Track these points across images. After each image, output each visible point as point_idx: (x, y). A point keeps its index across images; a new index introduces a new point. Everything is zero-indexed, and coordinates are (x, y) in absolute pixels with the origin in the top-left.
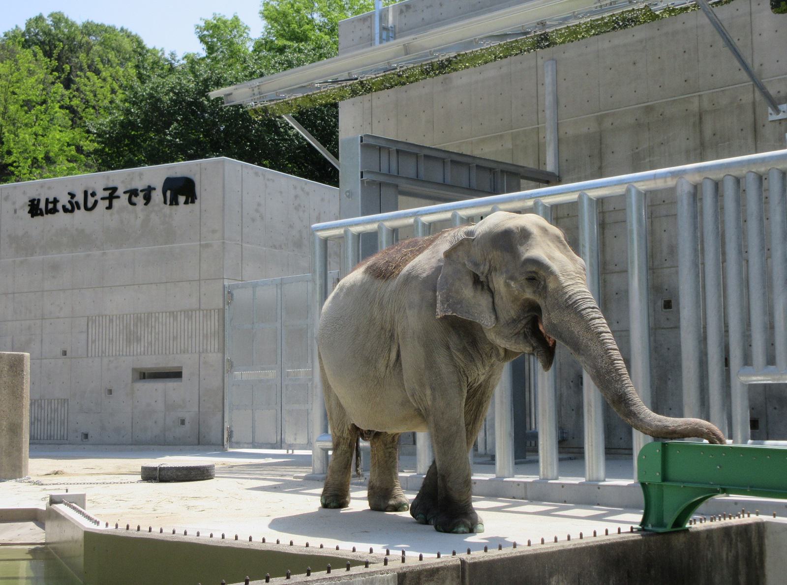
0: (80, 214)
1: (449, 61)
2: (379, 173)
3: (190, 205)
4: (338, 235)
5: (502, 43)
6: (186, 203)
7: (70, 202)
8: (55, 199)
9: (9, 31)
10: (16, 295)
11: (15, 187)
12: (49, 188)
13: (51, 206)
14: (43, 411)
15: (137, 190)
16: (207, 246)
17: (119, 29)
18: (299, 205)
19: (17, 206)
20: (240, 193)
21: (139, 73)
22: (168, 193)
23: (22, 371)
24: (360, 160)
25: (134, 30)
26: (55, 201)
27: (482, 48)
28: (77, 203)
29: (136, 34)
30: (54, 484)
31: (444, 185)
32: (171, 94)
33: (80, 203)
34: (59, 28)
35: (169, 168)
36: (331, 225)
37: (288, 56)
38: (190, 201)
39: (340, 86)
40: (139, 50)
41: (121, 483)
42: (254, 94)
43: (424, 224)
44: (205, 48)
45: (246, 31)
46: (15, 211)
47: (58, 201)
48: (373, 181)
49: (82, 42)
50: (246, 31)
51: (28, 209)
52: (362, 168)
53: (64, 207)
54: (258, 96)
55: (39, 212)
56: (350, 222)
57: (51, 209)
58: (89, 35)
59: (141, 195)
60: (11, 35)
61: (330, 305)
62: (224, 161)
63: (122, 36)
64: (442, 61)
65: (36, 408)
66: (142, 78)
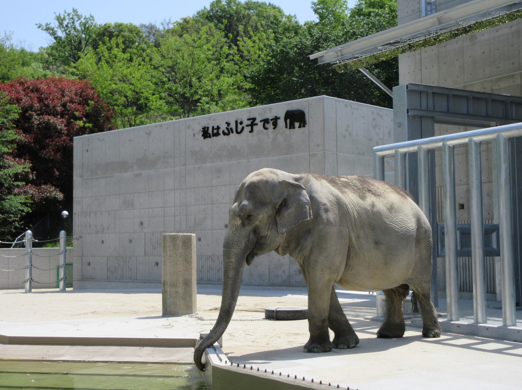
0: (233, 136)
1: (470, 27)
2: (421, 110)
3: (302, 128)
4: (391, 154)
5: (508, 13)
6: (300, 127)
7: (227, 128)
8: (218, 126)
9: (200, 11)
10: (196, 189)
11: (194, 120)
12: (214, 120)
13: (215, 131)
14: (214, 263)
15: (268, 119)
16: (314, 155)
17: (268, 4)
18: (376, 125)
19: (195, 132)
20: (335, 119)
21: (276, 37)
22: (288, 121)
23: (191, 245)
24: (406, 101)
25: (277, 4)
26: (218, 128)
27: (493, 17)
28: (231, 129)
29: (279, 6)
30: (210, 320)
31: (468, 115)
32: (295, 49)
33: (233, 129)
34: (230, 7)
35: (288, 104)
36: (386, 148)
37: (372, 20)
38: (302, 126)
39: (395, 48)
40: (275, 21)
41: (252, 320)
42: (338, 56)
43: (449, 147)
44: (319, 17)
45: (345, 3)
46: (194, 135)
47: (220, 128)
48: (417, 115)
49: (245, 14)
50: (345, 3)
51: (202, 133)
52: (408, 107)
53: (223, 132)
54: (341, 57)
55: (208, 135)
56: (399, 145)
57: (215, 133)
58: (249, 9)
59: (271, 122)
60: (201, 13)
62: (323, 98)
63: (270, 9)
64: (465, 27)
65: (210, 261)
66: (277, 40)
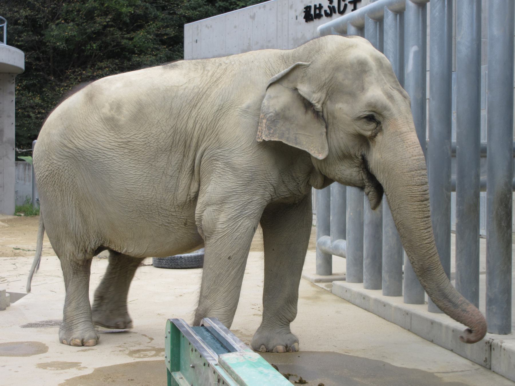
8: (320, 5)
28: (334, 7)
51: (303, 14)
53: (325, 11)
61: (369, 167)
